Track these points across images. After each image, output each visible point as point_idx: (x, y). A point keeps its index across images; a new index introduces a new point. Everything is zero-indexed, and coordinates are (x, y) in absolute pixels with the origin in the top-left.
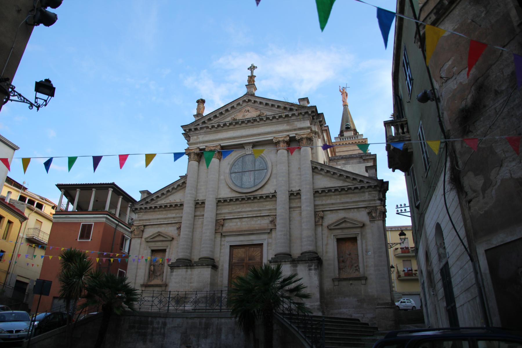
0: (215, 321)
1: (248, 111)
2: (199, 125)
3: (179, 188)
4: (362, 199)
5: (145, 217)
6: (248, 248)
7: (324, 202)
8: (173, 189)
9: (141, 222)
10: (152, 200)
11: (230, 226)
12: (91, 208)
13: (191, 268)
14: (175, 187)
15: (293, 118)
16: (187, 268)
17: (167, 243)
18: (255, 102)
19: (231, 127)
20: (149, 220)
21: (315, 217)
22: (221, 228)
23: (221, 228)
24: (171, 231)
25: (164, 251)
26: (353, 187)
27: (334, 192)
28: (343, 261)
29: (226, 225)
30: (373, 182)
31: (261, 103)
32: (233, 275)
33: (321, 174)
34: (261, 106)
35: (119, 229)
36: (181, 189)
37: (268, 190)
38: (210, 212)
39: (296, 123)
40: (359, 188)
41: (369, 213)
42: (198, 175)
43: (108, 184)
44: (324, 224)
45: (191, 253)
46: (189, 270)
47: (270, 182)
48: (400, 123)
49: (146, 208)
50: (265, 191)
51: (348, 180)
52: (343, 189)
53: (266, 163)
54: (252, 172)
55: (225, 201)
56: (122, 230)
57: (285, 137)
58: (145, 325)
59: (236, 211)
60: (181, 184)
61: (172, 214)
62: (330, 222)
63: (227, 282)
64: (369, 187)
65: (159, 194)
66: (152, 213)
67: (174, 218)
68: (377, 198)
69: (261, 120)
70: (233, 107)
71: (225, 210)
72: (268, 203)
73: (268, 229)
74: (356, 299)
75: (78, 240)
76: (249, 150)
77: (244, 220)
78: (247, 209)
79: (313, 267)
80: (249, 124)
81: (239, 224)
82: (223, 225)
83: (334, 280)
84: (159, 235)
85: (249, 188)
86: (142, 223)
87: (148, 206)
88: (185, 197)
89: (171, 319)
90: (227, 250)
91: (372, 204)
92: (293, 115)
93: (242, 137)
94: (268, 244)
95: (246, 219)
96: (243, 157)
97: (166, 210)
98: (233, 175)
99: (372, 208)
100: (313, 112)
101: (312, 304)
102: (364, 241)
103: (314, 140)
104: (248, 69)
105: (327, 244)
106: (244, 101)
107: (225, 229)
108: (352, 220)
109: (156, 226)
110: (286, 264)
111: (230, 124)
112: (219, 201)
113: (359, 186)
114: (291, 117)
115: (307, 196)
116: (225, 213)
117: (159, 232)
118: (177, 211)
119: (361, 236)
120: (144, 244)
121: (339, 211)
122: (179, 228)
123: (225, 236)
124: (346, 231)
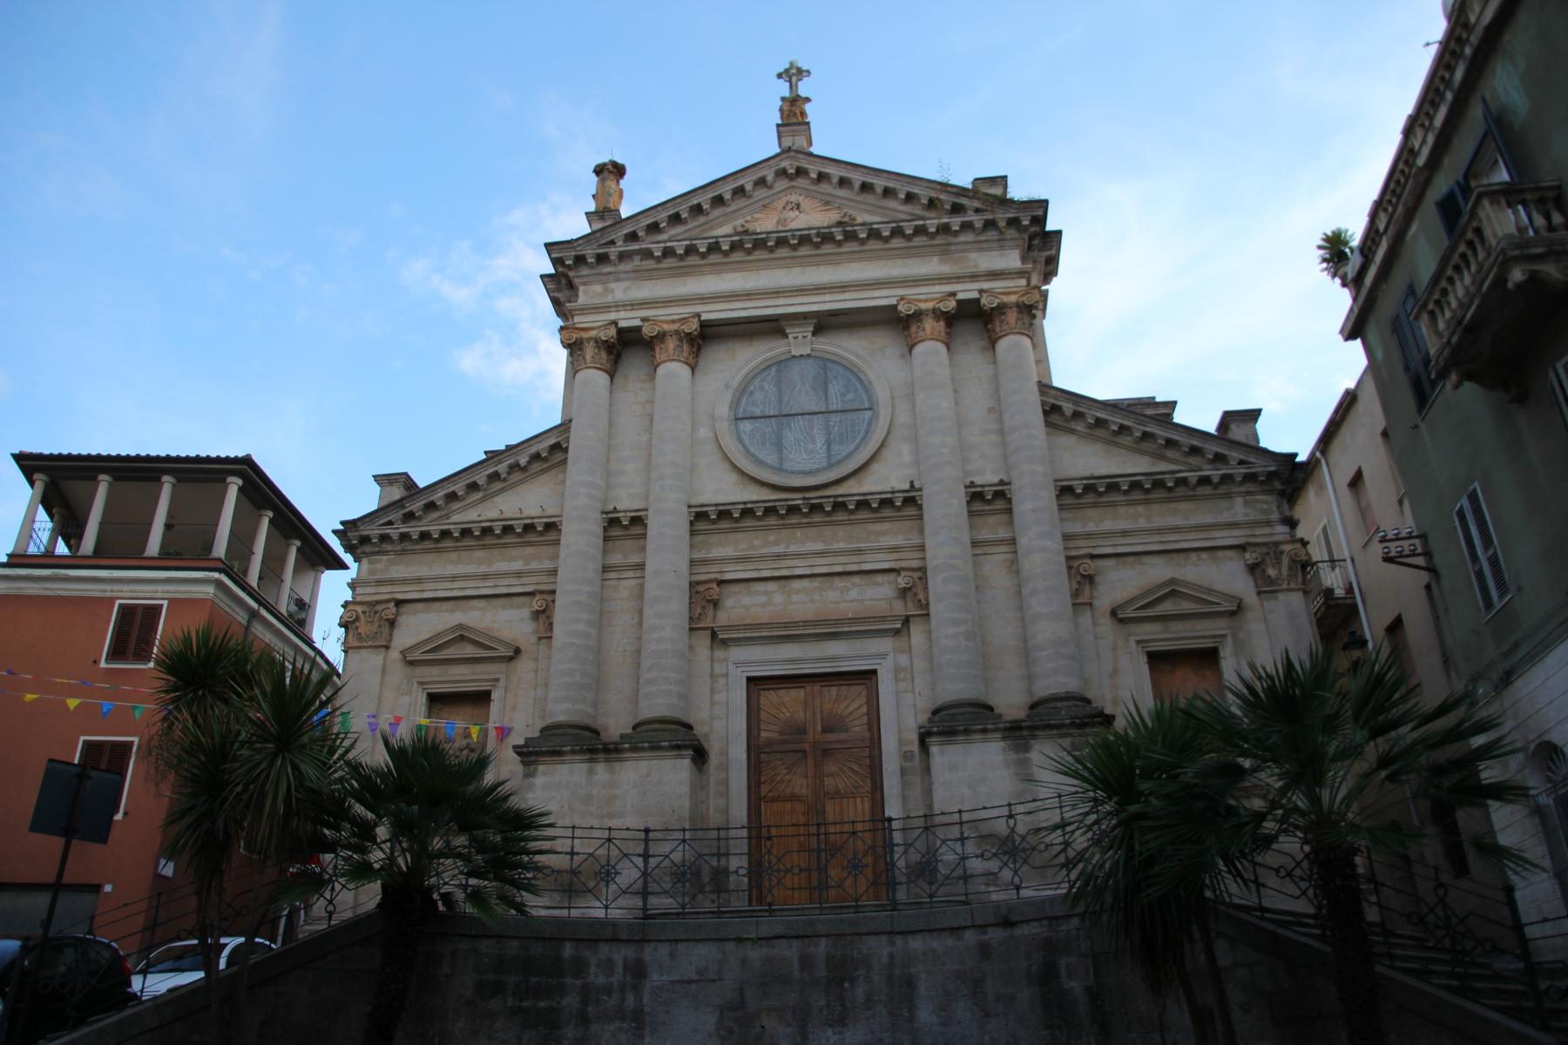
0: (880, 949)
1: (798, 206)
2: (612, 242)
3: (536, 466)
4: (1226, 517)
5: (401, 570)
6: (817, 687)
7: (1091, 527)
8: (515, 467)
9: (383, 589)
10: (431, 506)
11: (740, 607)
12: (154, 546)
13: (607, 760)
14: (523, 461)
15: (962, 238)
16: (591, 760)
18: (822, 177)
19: (738, 256)
20: (419, 580)
22: (710, 612)
24: (511, 623)
25: (481, 698)
26: (1193, 476)
27: (1125, 493)
29: (729, 602)
30: (1260, 462)
31: (843, 182)
32: (764, 789)
33: (1073, 431)
34: (843, 193)
35: (258, 630)
36: (543, 471)
37: (886, 478)
38: (667, 552)
39: (973, 255)
40: (1216, 480)
41: (1253, 569)
42: (611, 424)
43: (227, 460)
44: (1096, 603)
45: (595, 704)
46: (600, 768)
47: (885, 453)
48: (1536, 196)
49: (404, 537)
50: (871, 484)
51: (1170, 453)
53: (867, 388)
54: (818, 421)
55: (724, 514)
56: (268, 637)
57: (941, 300)
58: (543, 967)
59: (764, 551)
60: (546, 454)
61: (510, 562)
62: (1120, 595)
63: (744, 813)
64: (1250, 478)
65: (459, 487)
66: (429, 557)
67: (519, 574)
68: (1275, 516)
69: (850, 236)
70: (740, 192)
71: (725, 548)
72: (886, 526)
73: (895, 618)
75: (103, 664)
76: (800, 342)
77: (797, 584)
78: (806, 545)
80: (804, 251)
82: (716, 604)
84: (462, 638)
85: (811, 473)
86: (385, 592)
87: (414, 530)
88: (572, 498)
89: (665, 949)
90: (739, 695)
91: (1262, 535)
92: (967, 226)
93: (777, 293)
94: (897, 670)
95: (805, 583)
97: (484, 547)
98: (747, 426)
99: (1264, 550)
104: (780, 76)
106: (782, 173)
108: (1199, 588)
109: (446, 605)
110: (986, 741)
111: (735, 247)
113: (1215, 474)
114: (956, 234)
115: (1034, 504)
116: (723, 560)
117: (460, 626)
118: (529, 550)
120: (398, 673)
121: (1145, 559)
122: (543, 615)
123: (725, 643)
124: (1178, 628)
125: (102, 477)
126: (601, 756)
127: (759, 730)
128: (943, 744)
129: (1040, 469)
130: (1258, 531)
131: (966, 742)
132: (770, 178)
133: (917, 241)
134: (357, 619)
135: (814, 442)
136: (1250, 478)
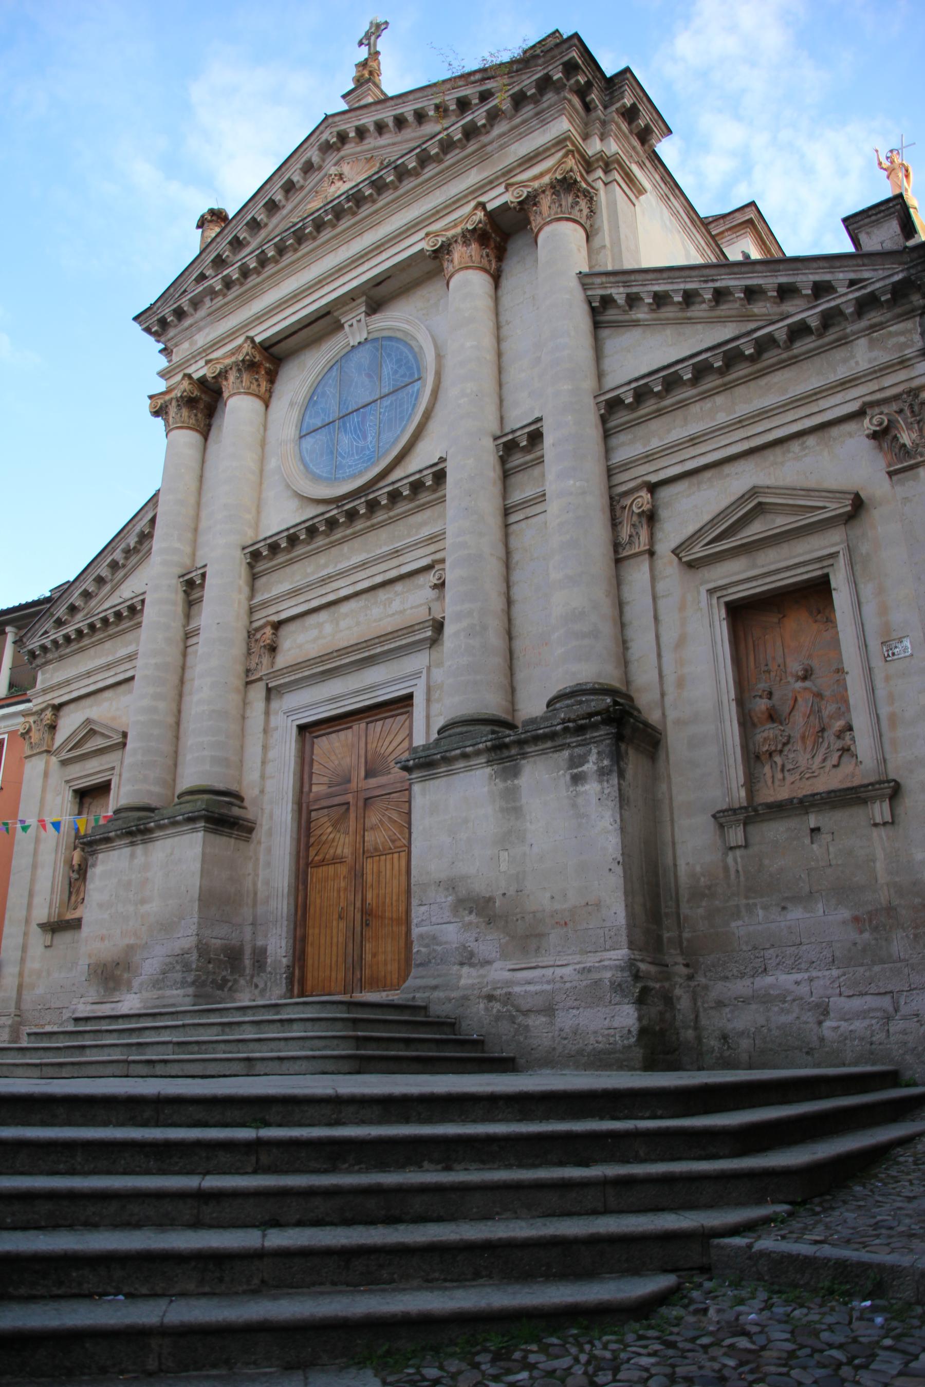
8: (128, 552)
11: (299, 644)
15: (496, 131)
16: (132, 844)
17: (109, 760)
20: (68, 682)
21: (615, 523)
23: (266, 660)
26: (779, 330)
28: (772, 716)
33: (635, 323)
40: (814, 323)
46: (139, 849)
52: (733, 358)
64: (866, 304)
66: (77, 657)
74: (845, 914)
76: (357, 328)
77: (345, 608)
79: (590, 767)
81: (328, 628)
83: (723, 818)
90: (286, 747)
92: (494, 116)
95: (352, 604)
96: (340, 362)
100: (570, 68)
101: (591, 960)
102: (867, 590)
103: (602, 196)
105: (681, 642)
107: (282, 660)
108: (791, 491)
110: (469, 769)
112: (256, 556)
119: (852, 564)
121: (728, 469)
124: (771, 559)
125: (8, 629)
126: (139, 838)
127: (311, 785)
128: (424, 779)
129: (567, 387)
130: (887, 381)
131: (449, 773)
132: (316, 159)
133: (450, 159)
134: (29, 731)
135: (365, 438)
136: (866, 304)
